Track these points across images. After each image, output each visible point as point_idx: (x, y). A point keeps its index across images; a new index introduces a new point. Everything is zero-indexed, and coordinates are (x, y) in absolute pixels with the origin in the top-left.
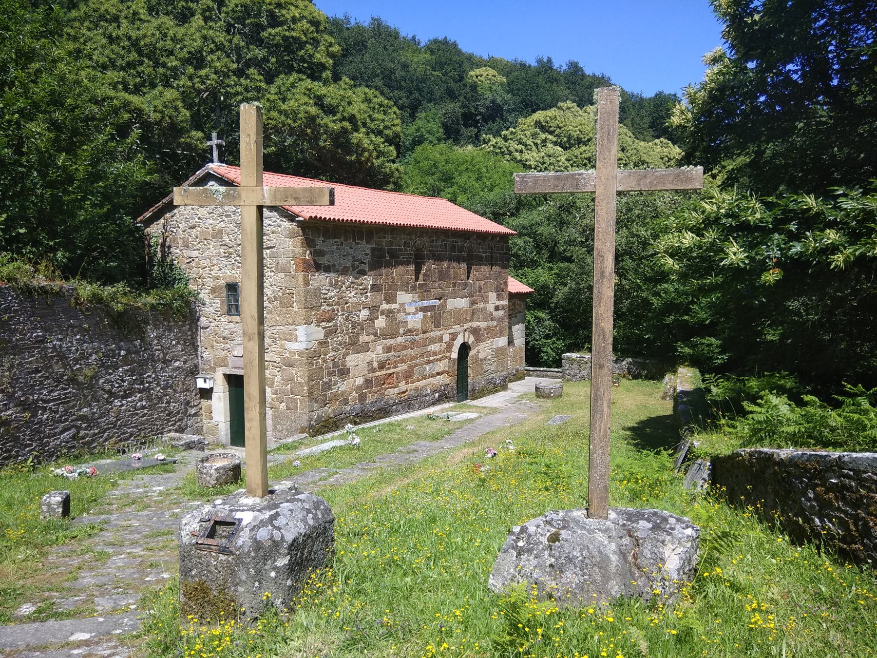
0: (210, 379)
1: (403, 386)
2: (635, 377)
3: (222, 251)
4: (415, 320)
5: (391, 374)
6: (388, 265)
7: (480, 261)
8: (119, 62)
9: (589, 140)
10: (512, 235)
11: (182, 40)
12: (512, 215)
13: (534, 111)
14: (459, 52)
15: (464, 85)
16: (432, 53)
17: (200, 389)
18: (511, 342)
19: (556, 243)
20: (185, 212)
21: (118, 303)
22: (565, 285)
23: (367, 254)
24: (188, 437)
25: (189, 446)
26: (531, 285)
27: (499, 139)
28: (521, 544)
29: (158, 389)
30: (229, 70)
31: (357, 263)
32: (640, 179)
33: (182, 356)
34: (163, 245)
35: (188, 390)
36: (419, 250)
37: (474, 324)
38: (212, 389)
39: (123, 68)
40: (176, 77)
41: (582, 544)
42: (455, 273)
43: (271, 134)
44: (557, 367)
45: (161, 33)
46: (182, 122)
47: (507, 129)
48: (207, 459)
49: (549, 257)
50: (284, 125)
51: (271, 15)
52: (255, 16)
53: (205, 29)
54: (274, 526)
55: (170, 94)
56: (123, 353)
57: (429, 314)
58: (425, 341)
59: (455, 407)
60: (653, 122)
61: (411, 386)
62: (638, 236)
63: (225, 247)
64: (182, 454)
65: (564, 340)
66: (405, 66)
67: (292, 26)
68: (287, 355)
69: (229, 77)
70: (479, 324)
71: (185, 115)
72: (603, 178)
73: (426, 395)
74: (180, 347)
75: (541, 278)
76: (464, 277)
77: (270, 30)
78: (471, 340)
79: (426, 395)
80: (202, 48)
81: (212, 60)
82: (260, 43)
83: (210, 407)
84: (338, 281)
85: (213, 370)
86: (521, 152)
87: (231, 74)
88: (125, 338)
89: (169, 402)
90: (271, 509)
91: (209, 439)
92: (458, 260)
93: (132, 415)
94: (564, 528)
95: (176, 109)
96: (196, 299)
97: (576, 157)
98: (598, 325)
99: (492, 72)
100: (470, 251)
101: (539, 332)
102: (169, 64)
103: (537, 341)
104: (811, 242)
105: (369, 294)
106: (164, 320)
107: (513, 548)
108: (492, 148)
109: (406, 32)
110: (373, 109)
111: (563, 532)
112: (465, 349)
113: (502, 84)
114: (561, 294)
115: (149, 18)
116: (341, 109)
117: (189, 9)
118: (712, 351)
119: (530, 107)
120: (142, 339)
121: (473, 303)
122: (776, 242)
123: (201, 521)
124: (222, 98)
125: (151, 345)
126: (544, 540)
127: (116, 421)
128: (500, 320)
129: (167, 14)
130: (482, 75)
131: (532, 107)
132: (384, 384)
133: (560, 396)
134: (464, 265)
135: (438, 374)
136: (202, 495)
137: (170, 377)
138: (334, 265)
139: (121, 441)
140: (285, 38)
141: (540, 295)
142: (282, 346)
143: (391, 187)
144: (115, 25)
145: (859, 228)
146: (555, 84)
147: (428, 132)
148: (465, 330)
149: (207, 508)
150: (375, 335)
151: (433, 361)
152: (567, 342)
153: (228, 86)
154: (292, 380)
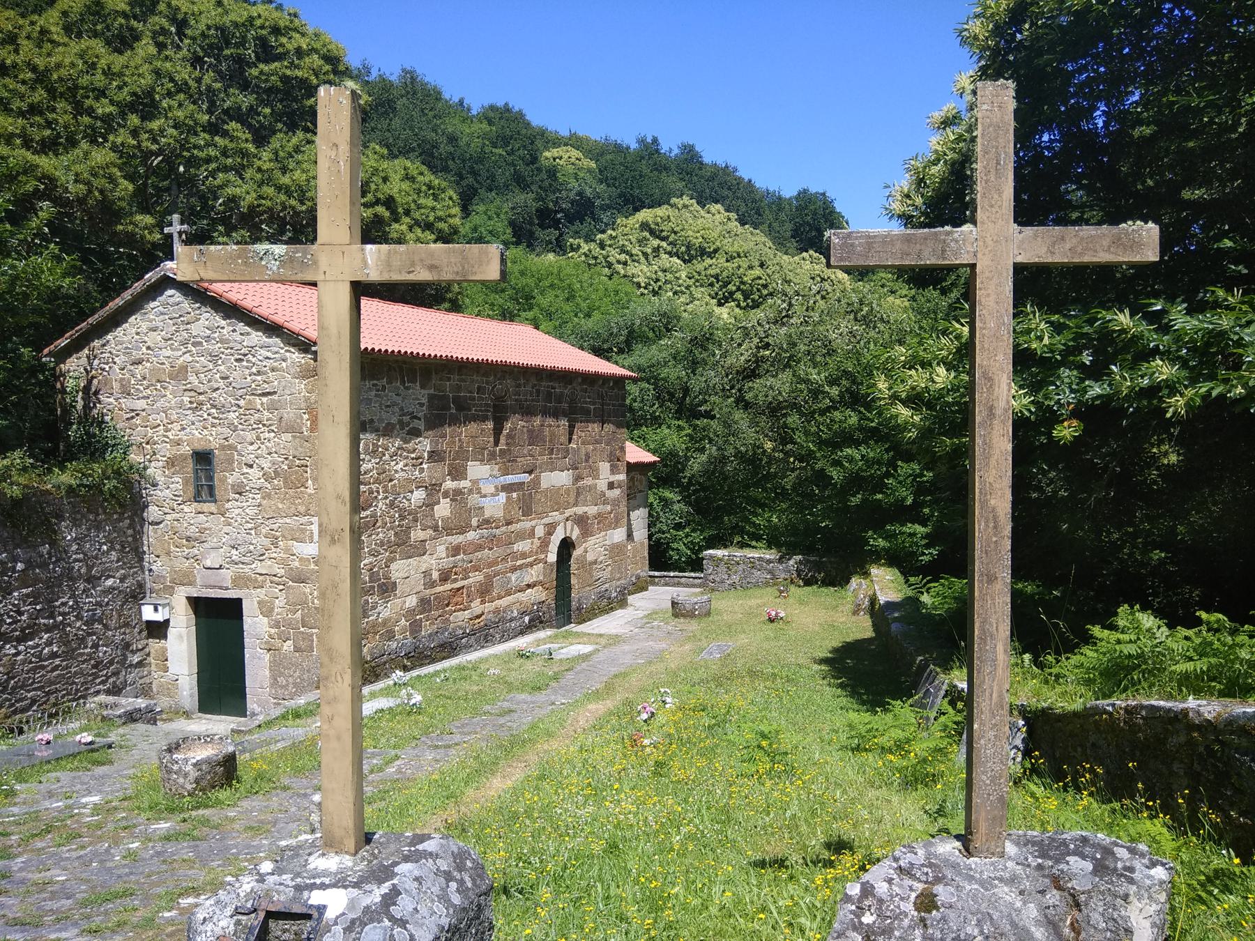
0: (164, 606)
1: (476, 607)
2: (808, 583)
3: (186, 399)
4: (495, 505)
5: (459, 589)
6: (454, 421)
7: (587, 416)
8: (16, 104)
9: (716, 251)
10: (630, 378)
11: (121, 74)
12: (621, 351)
13: (637, 210)
14: (528, 125)
15: (539, 169)
16: (490, 123)
17: (148, 622)
18: (630, 536)
19: (686, 391)
20: (125, 339)
21: (12, 484)
22: (702, 450)
23: (422, 405)
24: (128, 702)
25: (132, 717)
26: (654, 452)
27: (592, 245)
28: (868, 919)
29: (78, 624)
30: (196, 124)
31: (406, 419)
32: (1054, 244)
33: (117, 569)
34: (86, 389)
35: (127, 625)
36: (500, 399)
37: (580, 510)
38: (167, 622)
39: (21, 114)
40: (111, 130)
41: (978, 911)
42: (552, 435)
43: (262, 222)
44: (693, 570)
45: (86, 62)
46: (119, 199)
47: (603, 232)
48: (178, 746)
49: (677, 412)
50: (284, 208)
51: (263, 43)
52: (237, 46)
53: (158, 59)
54: (392, 918)
55: (101, 156)
56: (20, 566)
57: (515, 495)
58: (510, 537)
59: (556, 636)
60: (795, 230)
61: (489, 607)
62: (807, 381)
63: (193, 394)
64: (121, 731)
65: (702, 532)
66: (453, 139)
67: (296, 62)
68: (297, 564)
69: (196, 134)
70: (586, 509)
71: (126, 189)
72: (989, 240)
73: (511, 620)
74: (114, 555)
75: (668, 443)
76: (564, 439)
77: (262, 66)
78: (575, 534)
79: (511, 620)
80: (153, 89)
81: (170, 107)
82: (245, 86)
83: (164, 650)
84: (378, 446)
85: (170, 590)
86: (625, 264)
87: (199, 129)
88: (25, 542)
89: (95, 646)
90: (380, 882)
91: (162, 703)
92: (556, 415)
93: (34, 670)
94: (938, 880)
95: (112, 179)
96: (141, 476)
97: (699, 273)
98: (984, 503)
99: (575, 153)
100: (572, 401)
101: (666, 520)
102: (100, 111)
103: (664, 533)
104: (1123, 380)
105: (425, 466)
106: (89, 511)
107: (855, 929)
108: (583, 258)
109: (451, 93)
110: (419, 192)
111: (939, 889)
112: (566, 547)
113: (590, 171)
114: (697, 464)
115: (66, 40)
116: (373, 186)
117: (132, 29)
118: (916, 544)
119: (633, 204)
120: (53, 543)
121: (578, 478)
122: (1066, 380)
123: (237, 912)
124: (182, 169)
125: (66, 552)
126: (909, 907)
127: (7, 681)
128: (616, 503)
129: (96, 35)
130: (565, 157)
131: (633, 203)
132: (447, 605)
133: (708, 614)
134: (564, 423)
135: (529, 586)
136: (171, 810)
137: (99, 604)
138: (372, 421)
139: (15, 713)
140: (285, 79)
141: (666, 466)
142: (287, 550)
143: (447, 305)
144: (11, 48)
145: (1213, 355)
146: (664, 174)
147: (490, 232)
148: (567, 520)
149: (247, 884)
150: (435, 528)
151: (520, 567)
152: (706, 534)
153: (195, 147)
154: (304, 603)
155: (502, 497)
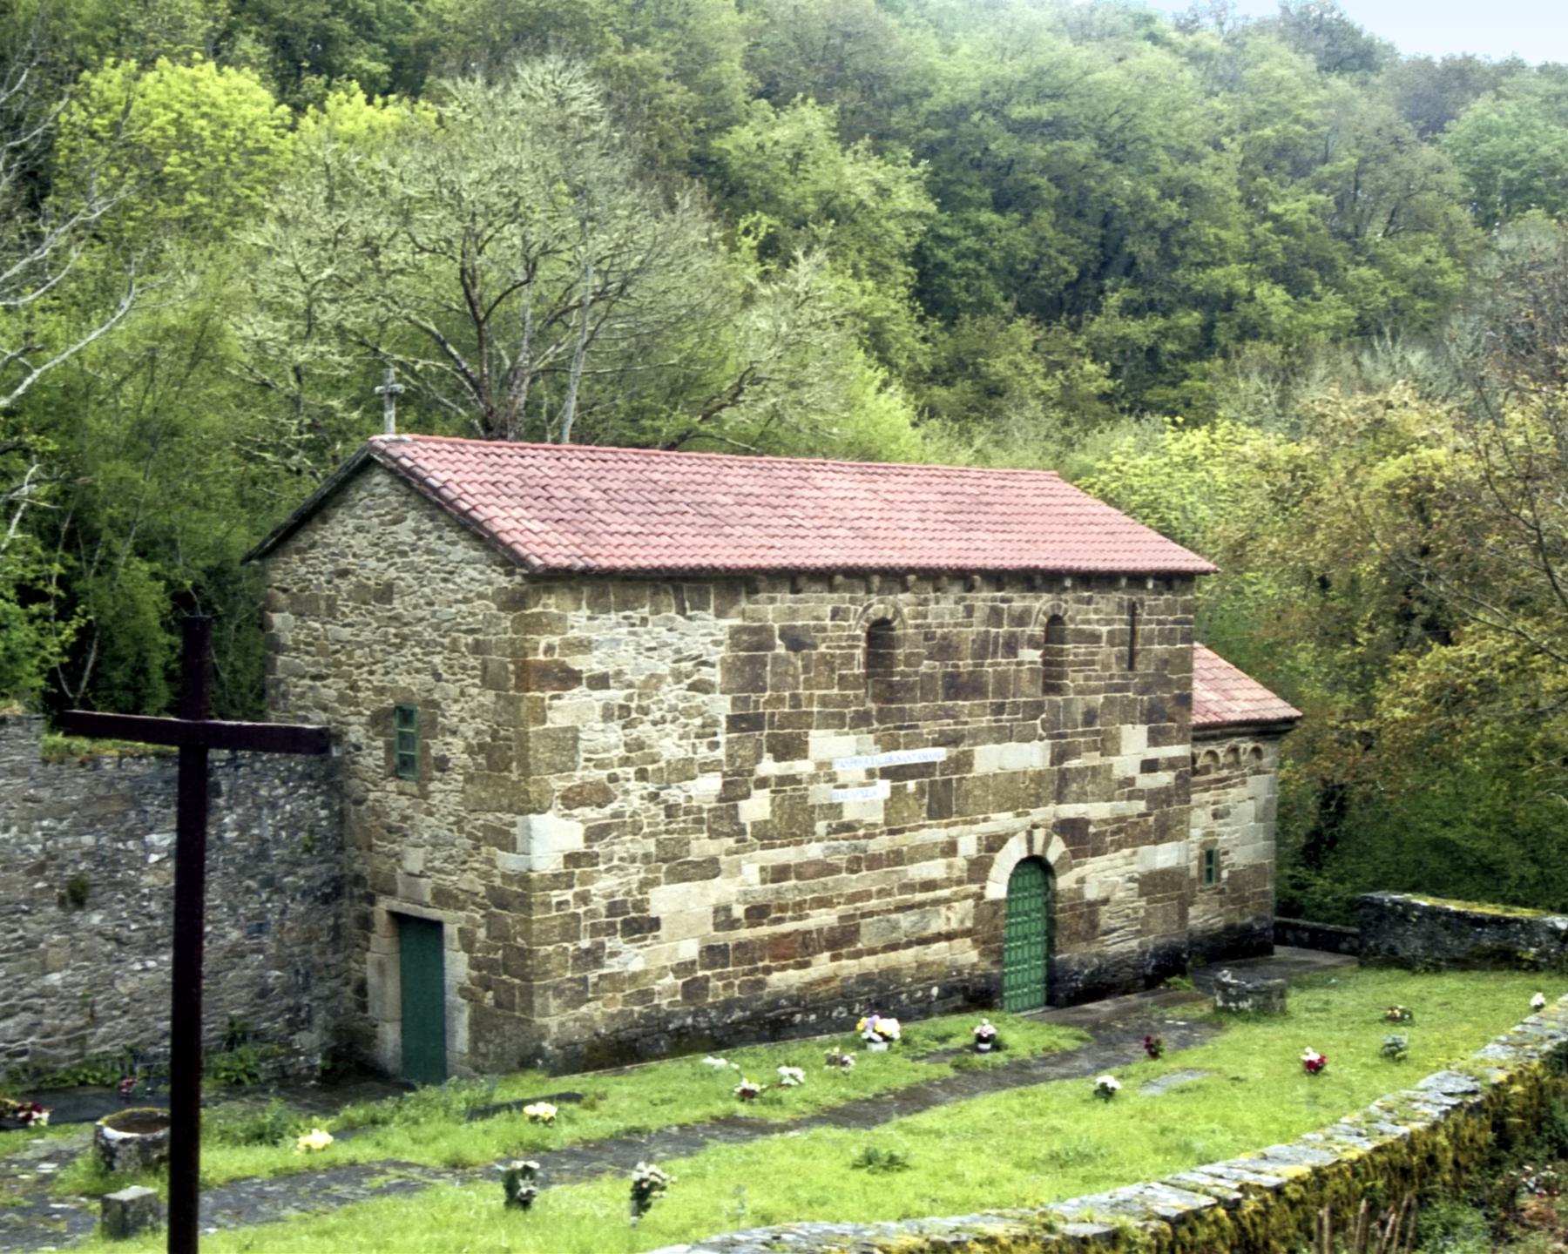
4: (866, 802)
31: (687, 666)
78: (1056, 851)
121: (1059, 756)
138: (619, 673)
155: (884, 788)
